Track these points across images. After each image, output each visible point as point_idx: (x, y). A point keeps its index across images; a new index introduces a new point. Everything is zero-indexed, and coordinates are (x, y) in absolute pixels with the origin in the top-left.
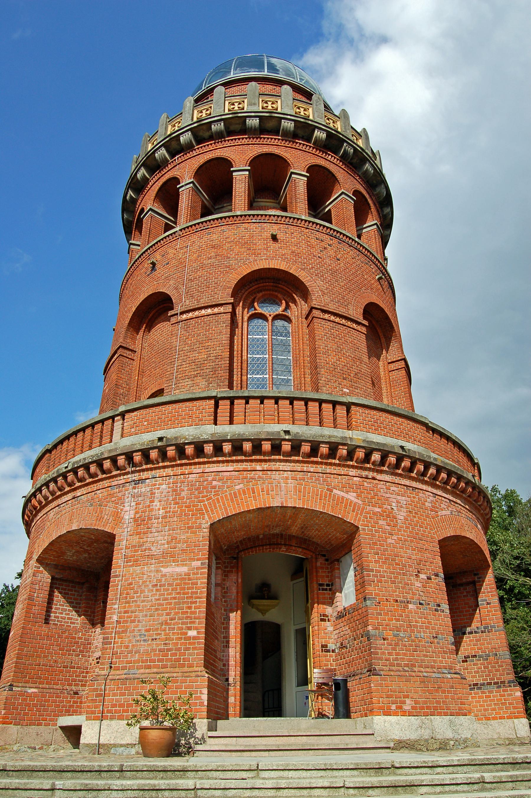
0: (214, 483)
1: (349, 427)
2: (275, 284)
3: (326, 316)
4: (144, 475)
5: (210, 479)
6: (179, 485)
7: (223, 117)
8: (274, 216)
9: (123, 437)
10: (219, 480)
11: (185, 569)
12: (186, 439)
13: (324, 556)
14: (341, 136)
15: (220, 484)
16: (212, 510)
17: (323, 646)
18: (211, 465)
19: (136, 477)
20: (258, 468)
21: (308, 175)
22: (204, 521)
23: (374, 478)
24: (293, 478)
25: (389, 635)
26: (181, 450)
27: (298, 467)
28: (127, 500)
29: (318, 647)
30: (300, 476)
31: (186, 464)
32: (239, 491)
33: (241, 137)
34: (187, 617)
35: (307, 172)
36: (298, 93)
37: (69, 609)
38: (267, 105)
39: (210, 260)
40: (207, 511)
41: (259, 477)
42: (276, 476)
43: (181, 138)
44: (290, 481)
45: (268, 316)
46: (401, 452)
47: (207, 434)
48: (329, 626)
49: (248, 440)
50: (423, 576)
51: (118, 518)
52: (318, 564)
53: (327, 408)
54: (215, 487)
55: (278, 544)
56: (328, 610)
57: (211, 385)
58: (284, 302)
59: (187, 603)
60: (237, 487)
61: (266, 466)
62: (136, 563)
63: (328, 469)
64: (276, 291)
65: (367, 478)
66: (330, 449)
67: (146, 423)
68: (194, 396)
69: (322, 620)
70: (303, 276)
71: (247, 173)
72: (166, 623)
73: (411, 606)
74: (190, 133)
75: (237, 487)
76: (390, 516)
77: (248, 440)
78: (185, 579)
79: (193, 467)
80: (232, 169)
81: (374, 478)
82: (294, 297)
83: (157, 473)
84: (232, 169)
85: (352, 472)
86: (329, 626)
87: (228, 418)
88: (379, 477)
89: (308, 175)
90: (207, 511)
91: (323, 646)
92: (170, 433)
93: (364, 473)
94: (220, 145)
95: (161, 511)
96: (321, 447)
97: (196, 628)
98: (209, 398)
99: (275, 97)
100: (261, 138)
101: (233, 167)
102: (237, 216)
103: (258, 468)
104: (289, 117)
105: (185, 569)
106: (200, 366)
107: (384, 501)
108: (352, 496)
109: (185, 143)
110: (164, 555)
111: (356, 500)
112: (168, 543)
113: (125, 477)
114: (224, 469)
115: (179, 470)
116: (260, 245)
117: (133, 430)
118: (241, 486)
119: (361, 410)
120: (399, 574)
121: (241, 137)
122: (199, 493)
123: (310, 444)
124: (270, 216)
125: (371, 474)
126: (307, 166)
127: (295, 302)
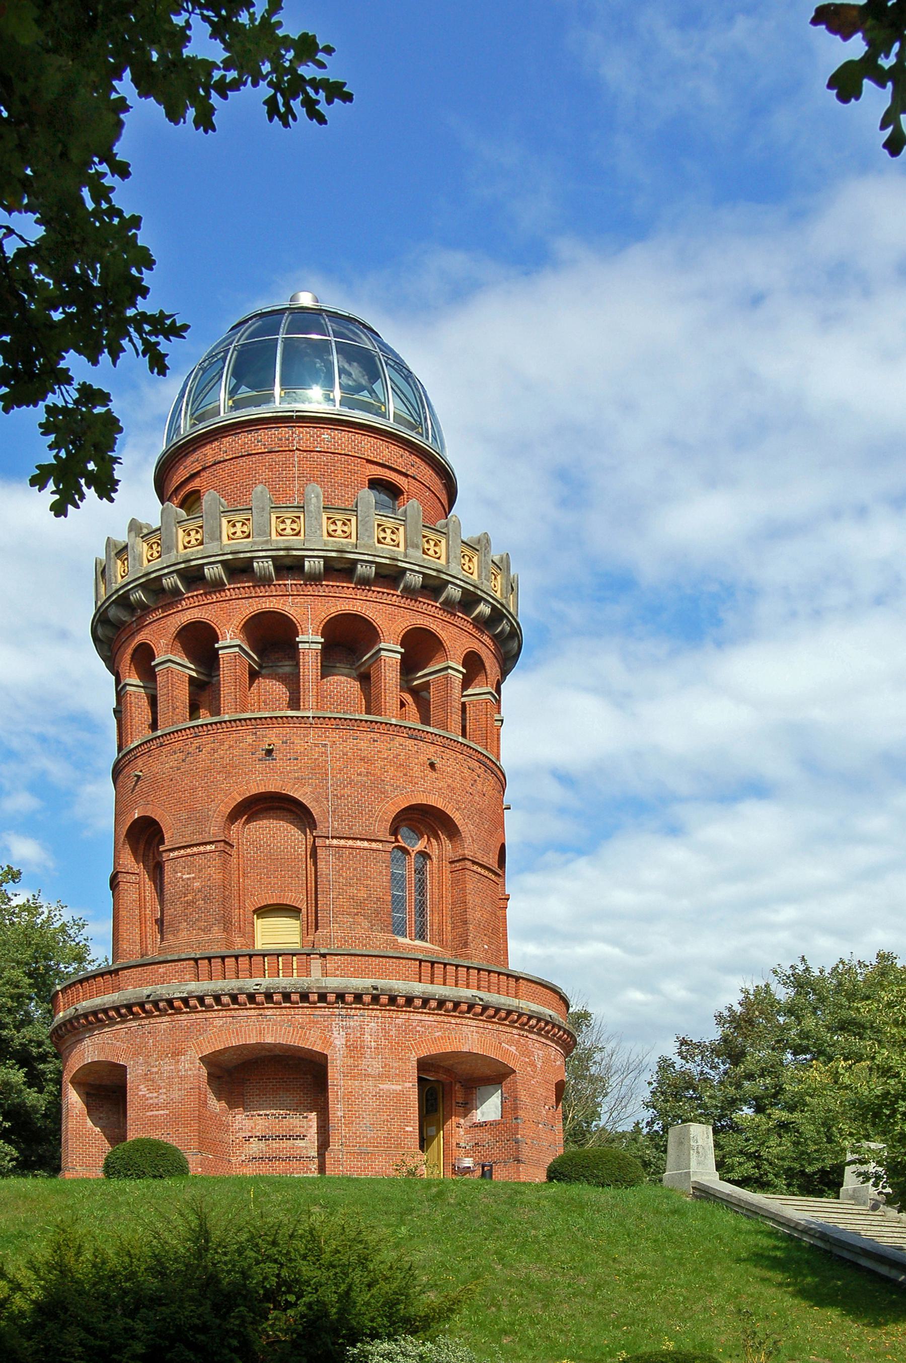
0: (418, 1028)
1: (516, 996)
2: (423, 818)
3: (475, 868)
4: (353, 1012)
5: (414, 1024)
6: (387, 1025)
7: (378, 560)
8: (432, 733)
10: (422, 1027)
11: (400, 1087)
12: (400, 993)
13: (460, 1082)
14: (504, 611)
15: (423, 1029)
16: (418, 1049)
17: (457, 1144)
18: (415, 1014)
19: (344, 1012)
20: (453, 1021)
21: (464, 671)
22: (412, 1056)
23: (527, 1037)
24: (476, 1032)
25: (529, 1141)
26: (393, 1000)
27: (481, 1024)
28: (335, 1029)
29: (454, 1144)
30: (481, 1030)
31: (394, 1010)
32: (438, 1037)
34: (404, 1119)
36: (429, 465)
39: (359, 778)
40: (414, 1048)
41: (453, 1028)
42: (465, 1028)
44: (474, 1034)
45: (411, 851)
46: (549, 1019)
47: (418, 992)
48: (461, 1131)
49: (451, 1001)
50: (547, 1107)
51: (327, 1042)
52: (456, 1088)
54: (419, 1032)
55: (429, 1071)
56: (462, 1121)
57: (374, 928)
58: (426, 836)
59: (403, 1110)
60: (437, 1034)
61: (458, 1020)
62: (354, 1078)
63: (501, 1028)
64: (419, 823)
65: (523, 1036)
67: (352, 969)
68: (402, 956)
69: (457, 1127)
70: (456, 817)
72: (387, 1121)
73: (540, 1125)
75: (437, 1034)
76: (533, 1064)
77: (451, 1001)
78: (399, 1095)
79: (399, 1013)
81: (527, 1037)
82: (438, 835)
83: (366, 1013)
85: (515, 1031)
86: (461, 1131)
88: (530, 1036)
90: (414, 1048)
91: (457, 1144)
92: (382, 983)
93: (522, 1032)
94: (360, 595)
95: (373, 1043)
97: (412, 1126)
98: (415, 960)
99: (439, 534)
100: (416, 601)
103: (453, 1021)
105: (400, 1087)
106: (361, 904)
107: (530, 1054)
108: (513, 1049)
110: (380, 1076)
111: (515, 1052)
112: (382, 1068)
113: (331, 1010)
114: (427, 1018)
115: (387, 1014)
116: (416, 771)
117: (338, 972)
118: (440, 1033)
119: (525, 982)
120: (536, 1104)
122: (406, 1034)
124: (428, 732)
125: (526, 1033)
127: (437, 838)
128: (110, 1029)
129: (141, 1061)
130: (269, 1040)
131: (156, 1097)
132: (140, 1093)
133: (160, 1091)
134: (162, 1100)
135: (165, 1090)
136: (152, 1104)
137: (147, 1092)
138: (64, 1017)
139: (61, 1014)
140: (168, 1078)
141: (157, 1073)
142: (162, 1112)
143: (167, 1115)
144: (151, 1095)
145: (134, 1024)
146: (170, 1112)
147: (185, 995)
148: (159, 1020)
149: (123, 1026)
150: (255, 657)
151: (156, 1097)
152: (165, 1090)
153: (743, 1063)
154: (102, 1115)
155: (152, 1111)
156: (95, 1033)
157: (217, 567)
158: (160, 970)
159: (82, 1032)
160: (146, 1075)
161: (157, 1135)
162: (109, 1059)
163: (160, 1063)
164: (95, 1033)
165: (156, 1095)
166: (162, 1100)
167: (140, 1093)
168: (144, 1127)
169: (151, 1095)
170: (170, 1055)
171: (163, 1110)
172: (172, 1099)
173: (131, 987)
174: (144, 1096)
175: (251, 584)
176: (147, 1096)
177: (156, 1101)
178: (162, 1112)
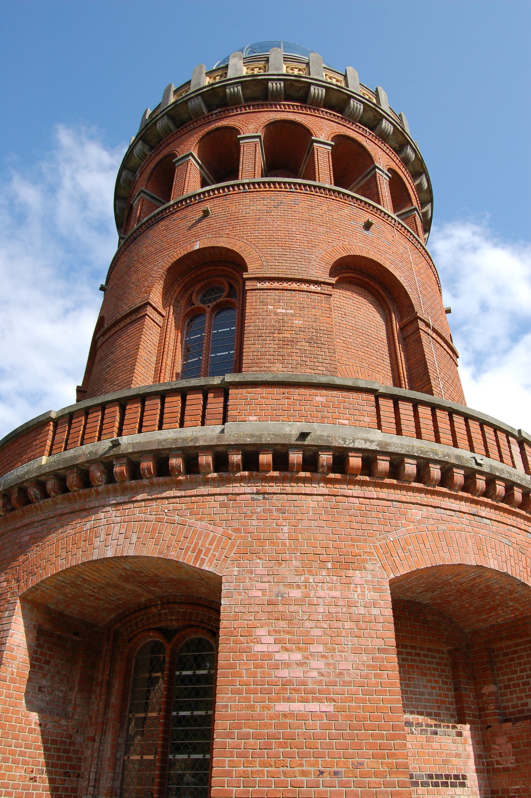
9: (141, 432)
21: (333, 143)
33: (325, 110)
35: (331, 141)
37: (523, 642)
38: (292, 72)
43: (189, 104)
53: (442, 416)
66: (391, 464)
71: (330, 148)
74: (200, 98)
80: (239, 136)
84: (239, 136)
87: (221, 416)
89: (333, 143)
96: (380, 460)
101: (240, 134)
102: (243, 185)
104: (321, 83)
109: (384, 130)
121: (325, 110)
123: (389, 458)
126: (333, 135)
128: (183, 493)
129: (260, 570)
130: (493, 564)
131: (299, 664)
132: (258, 648)
133: (312, 648)
134: (315, 674)
135: (320, 648)
136: (290, 682)
137: (277, 647)
138: (48, 464)
139: (44, 460)
140: (329, 617)
141: (299, 602)
142: (314, 707)
143: (329, 716)
144: (285, 656)
145: (248, 490)
146: (338, 710)
147: (374, 447)
148: (308, 488)
149: (218, 490)
150: (212, 178)
151: (299, 664)
152: (320, 648)
153: (451, 703)
154: (44, 682)
155: (289, 700)
156: (139, 497)
157: (280, 84)
158: (318, 399)
159: (180, 482)
160: (270, 603)
161: (304, 774)
162: (173, 555)
163: (306, 581)
164: (139, 497)
165: (297, 656)
166: (315, 674)
167: (258, 648)
168: (268, 747)
169: (285, 656)
170: (329, 565)
171: (320, 701)
172: (341, 674)
173: (255, 418)
174: (268, 656)
175: (299, 104)
176: (277, 656)
177: (298, 673)
178: (314, 707)
